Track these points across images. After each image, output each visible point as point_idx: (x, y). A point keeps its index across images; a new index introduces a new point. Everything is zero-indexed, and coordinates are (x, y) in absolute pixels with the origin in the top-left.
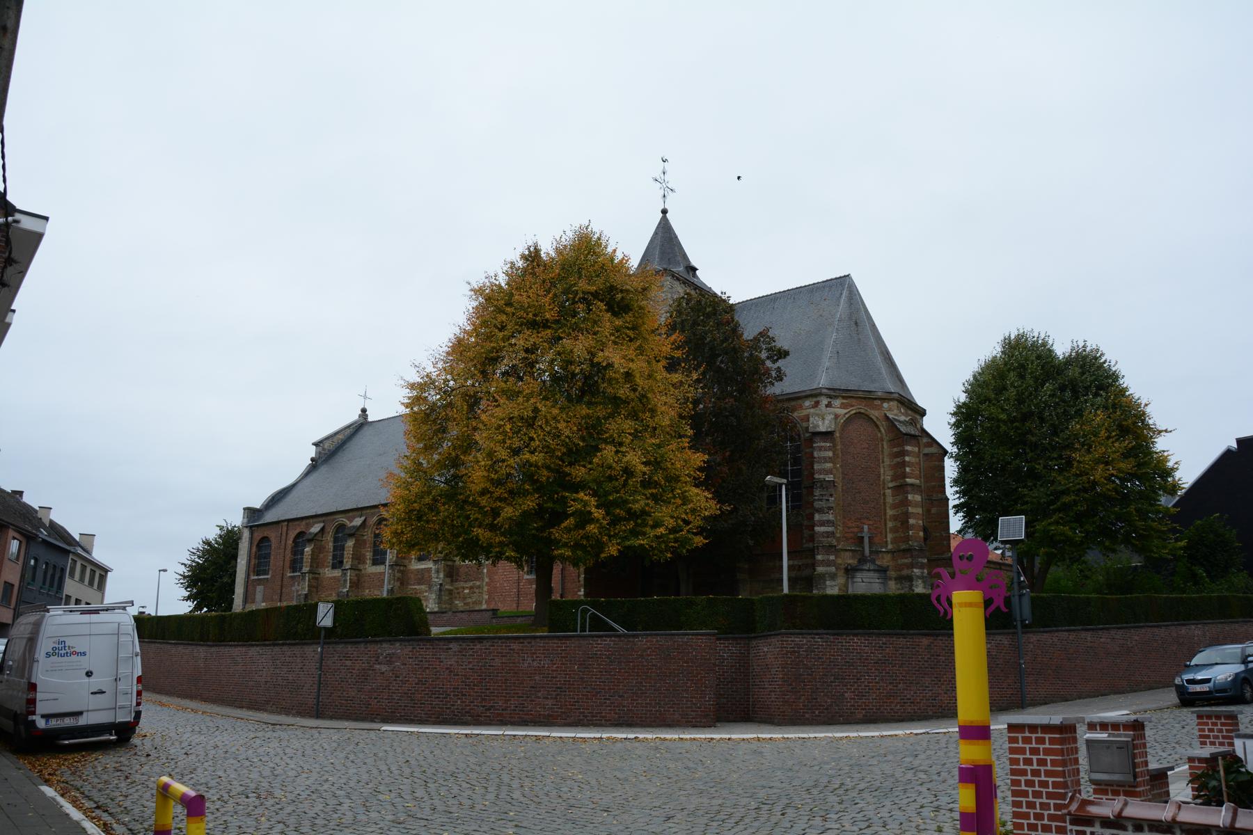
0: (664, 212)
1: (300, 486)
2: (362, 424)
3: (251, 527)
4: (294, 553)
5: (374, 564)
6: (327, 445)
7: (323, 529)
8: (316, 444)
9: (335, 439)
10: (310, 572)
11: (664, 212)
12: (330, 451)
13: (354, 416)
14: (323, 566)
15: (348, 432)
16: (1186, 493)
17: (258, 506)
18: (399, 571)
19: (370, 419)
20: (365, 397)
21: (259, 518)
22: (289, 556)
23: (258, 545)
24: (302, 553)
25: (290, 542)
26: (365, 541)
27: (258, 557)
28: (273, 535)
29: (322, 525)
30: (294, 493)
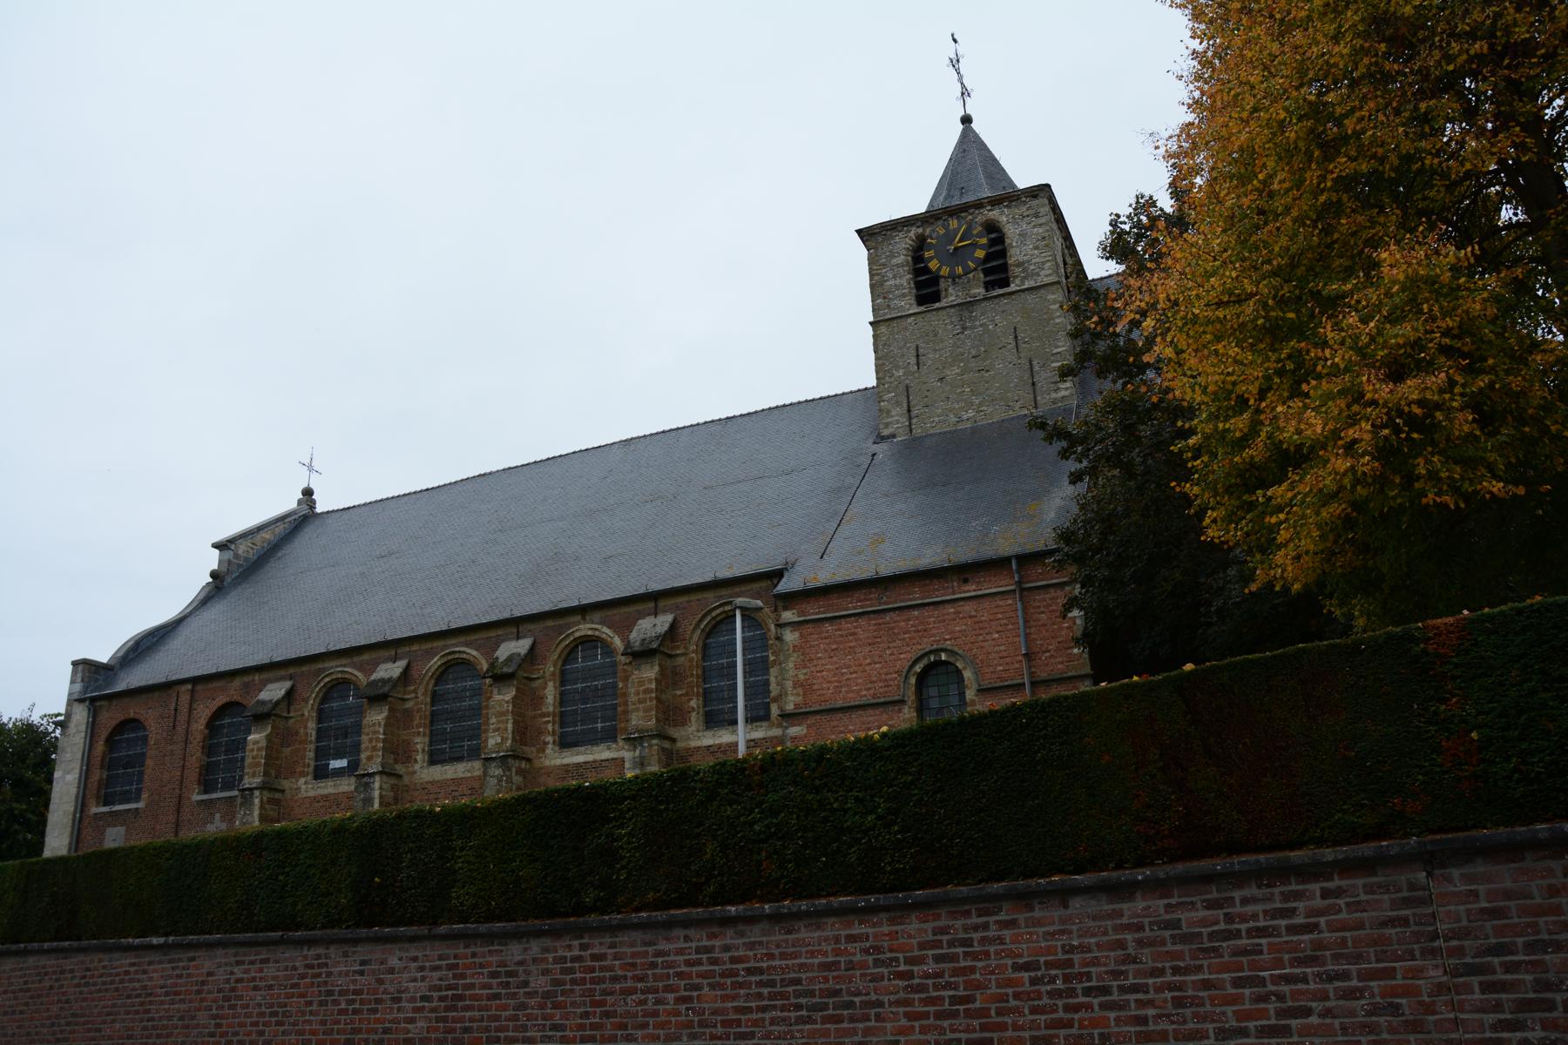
0: (967, 120)
1: (194, 623)
2: (304, 518)
3: (93, 700)
4: (209, 749)
5: (433, 761)
6: (242, 549)
7: (290, 694)
8: (216, 546)
9: (258, 538)
10: (262, 788)
11: (967, 120)
12: (247, 562)
13: (288, 502)
14: (292, 773)
15: (280, 529)
16: (771, 767)
17: (103, 656)
18: (520, 771)
19: (319, 510)
20: (310, 468)
21: (109, 681)
22: (196, 756)
23: (109, 740)
24: (240, 745)
25: (200, 725)
26: (408, 714)
27: (109, 764)
28: (152, 716)
29: (288, 684)
30: (176, 644)
